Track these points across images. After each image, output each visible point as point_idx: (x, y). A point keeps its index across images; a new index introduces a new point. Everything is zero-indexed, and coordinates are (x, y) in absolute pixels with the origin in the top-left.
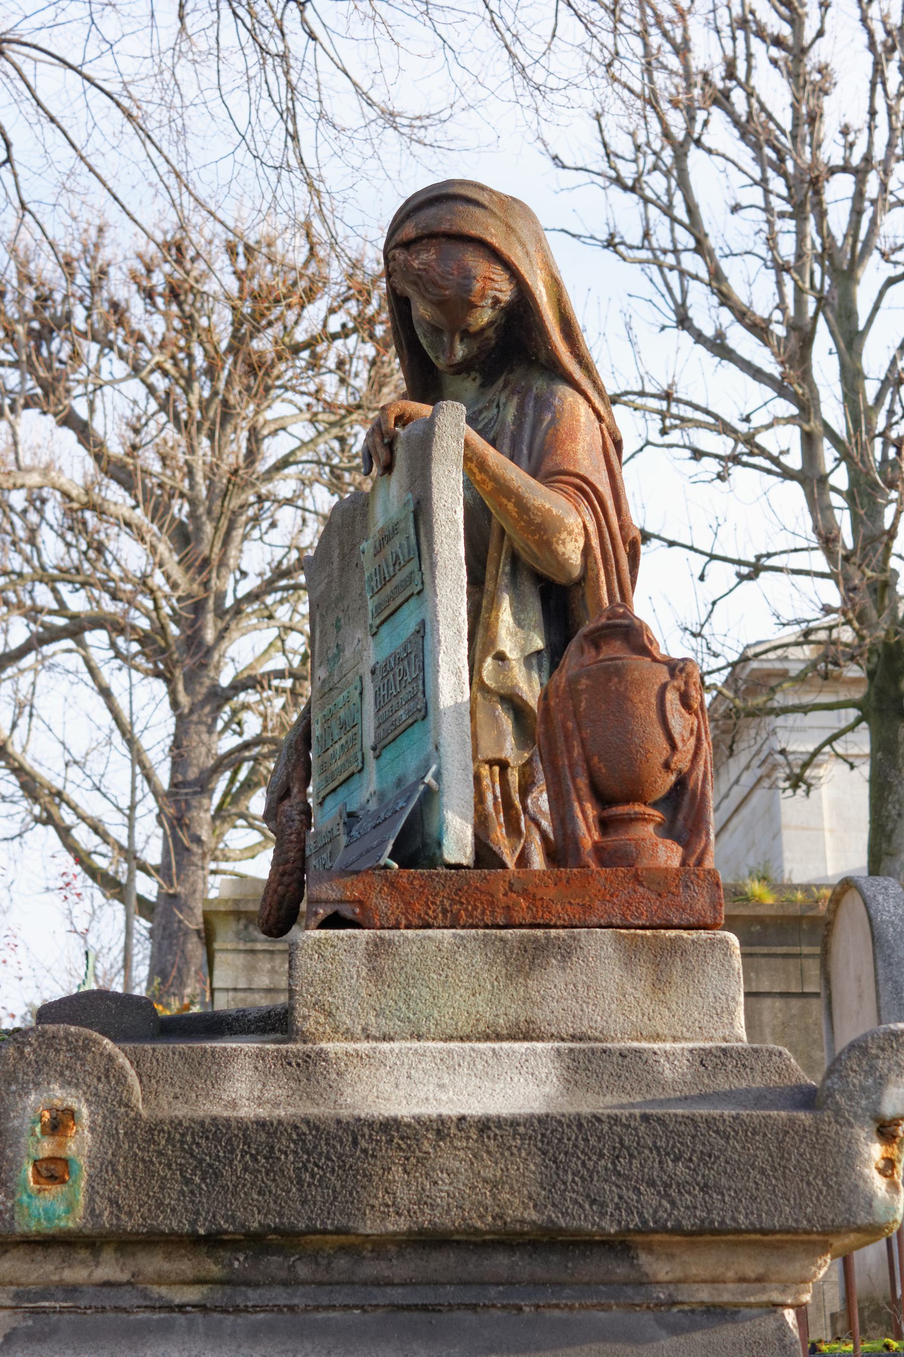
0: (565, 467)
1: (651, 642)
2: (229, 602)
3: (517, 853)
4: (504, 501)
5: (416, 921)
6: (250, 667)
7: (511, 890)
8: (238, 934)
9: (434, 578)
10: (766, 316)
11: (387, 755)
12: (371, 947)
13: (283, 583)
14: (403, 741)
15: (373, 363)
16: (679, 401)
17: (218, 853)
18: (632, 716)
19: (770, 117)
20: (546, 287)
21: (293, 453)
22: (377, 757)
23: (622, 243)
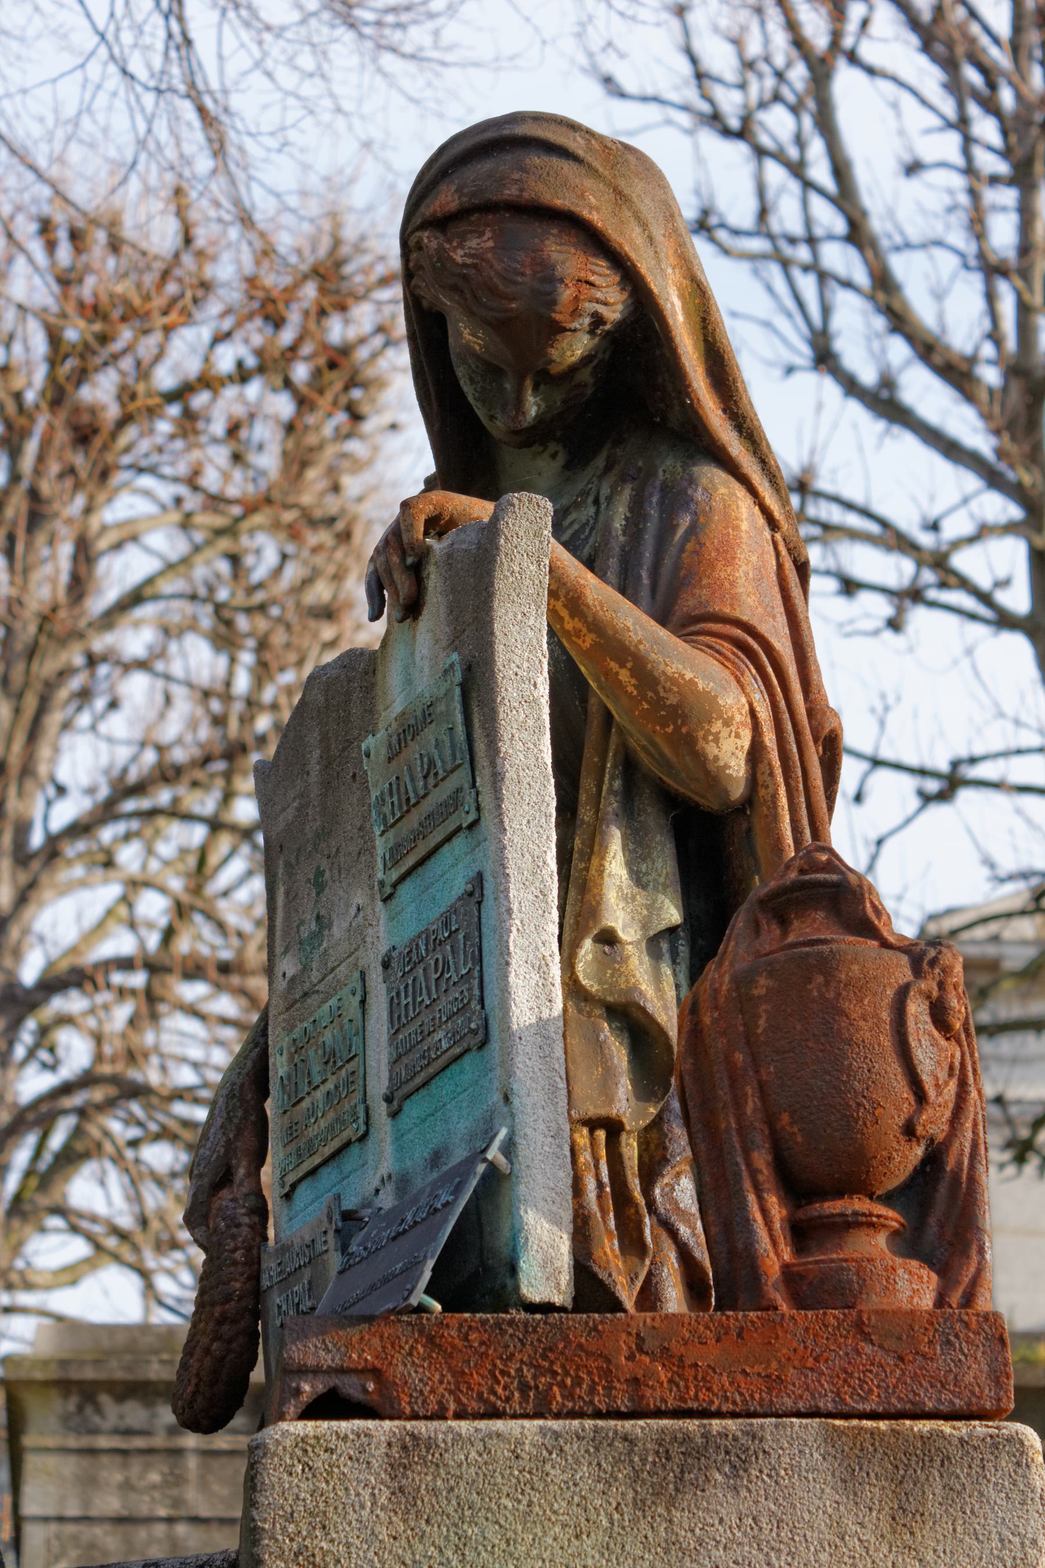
0: (717, 607)
1: (878, 911)
2: (37, 839)
3: (639, 1284)
4: (613, 665)
5: (474, 1405)
6: (74, 950)
7: (641, 1350)
8: (65, 1420)
9: (498, 799)
10: (968, 349)
11: (413, 1110)
12: (395, 1452)
13: (130, 805)
14: (443, 1087)
15: (290, 428)
16: (819, 495)
17: (14, 1277)
18: (849, 1042)
19: (973, 14)
20: (681, 297)
21: (150, 581)
22: (394, 1115)
23: (723, 225)
